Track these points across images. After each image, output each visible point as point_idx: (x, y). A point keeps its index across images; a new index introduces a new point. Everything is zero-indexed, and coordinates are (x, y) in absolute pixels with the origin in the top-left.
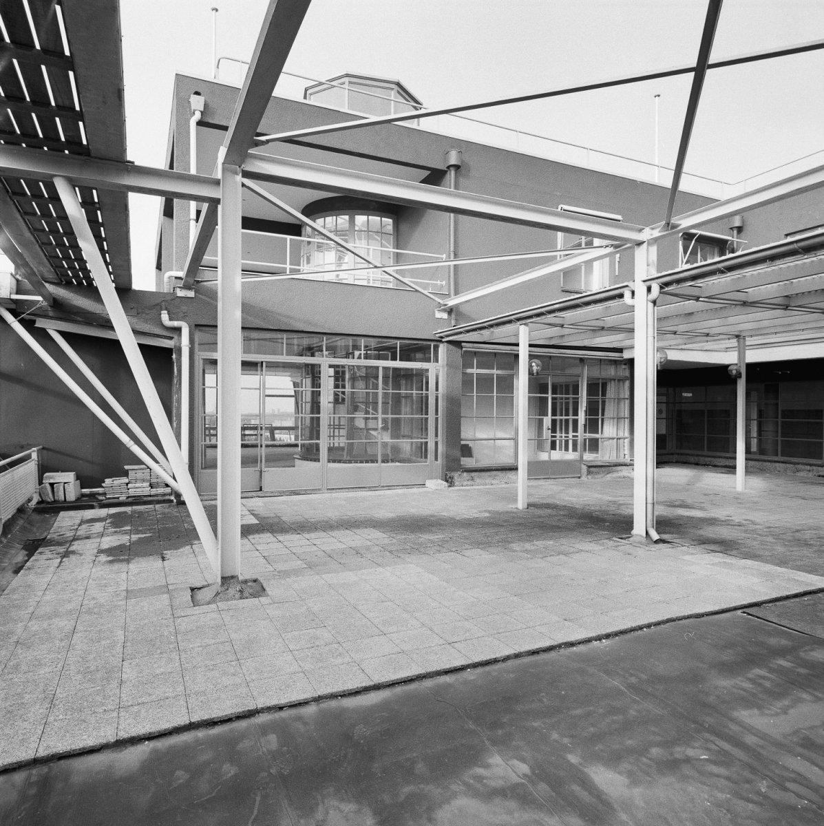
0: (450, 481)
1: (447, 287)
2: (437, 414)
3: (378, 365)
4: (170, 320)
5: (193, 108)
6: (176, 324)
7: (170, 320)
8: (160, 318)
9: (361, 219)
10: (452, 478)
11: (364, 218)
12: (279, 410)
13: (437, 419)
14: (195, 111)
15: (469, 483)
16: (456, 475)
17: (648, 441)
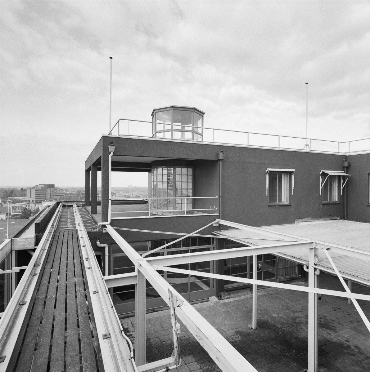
0: (219, 297)
1: (218, 199)
2: (214, 267)
3: (188, 249)
4: (101, 243)
5: (110, 151)
6: (103, 245)
7: (101, 243)
8: (96, 243)
9: (179, 170)
10: (220, 295)
11: (180, 169)
12: (132, 186)
13: (214, 269)
14: (110, 152)
15: (228, 296)
16: (222, 294)
17: (315, 303)
